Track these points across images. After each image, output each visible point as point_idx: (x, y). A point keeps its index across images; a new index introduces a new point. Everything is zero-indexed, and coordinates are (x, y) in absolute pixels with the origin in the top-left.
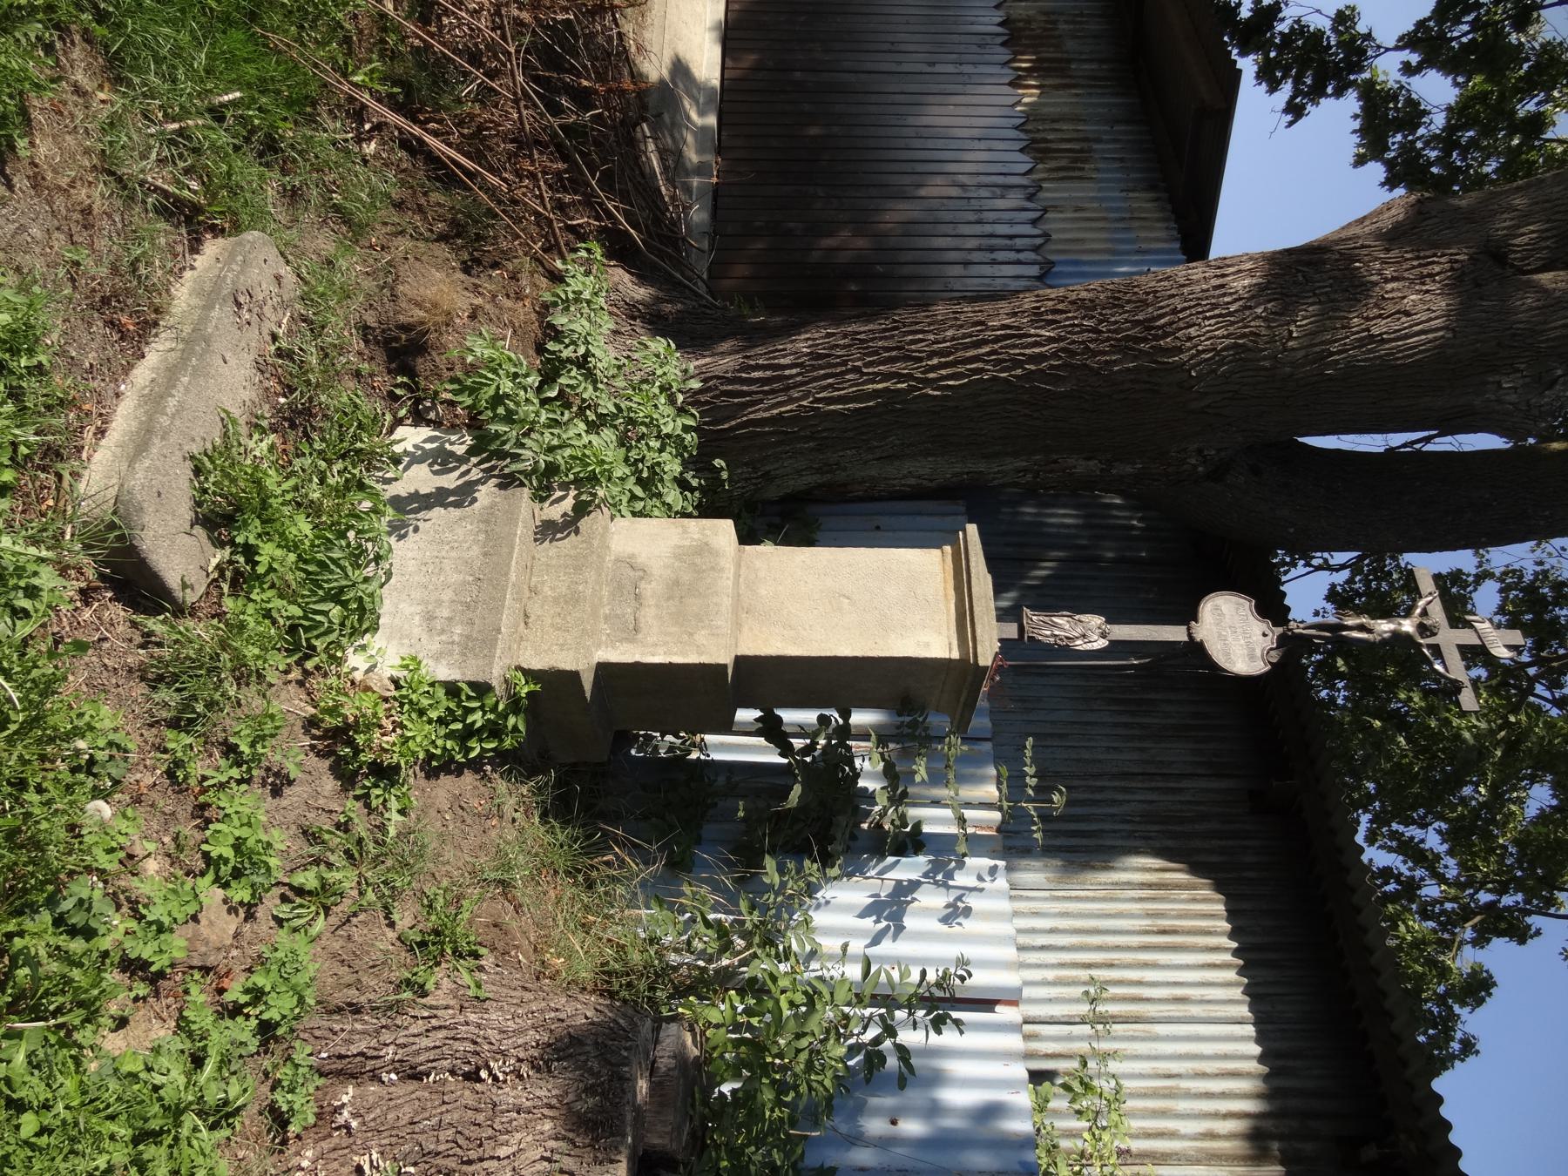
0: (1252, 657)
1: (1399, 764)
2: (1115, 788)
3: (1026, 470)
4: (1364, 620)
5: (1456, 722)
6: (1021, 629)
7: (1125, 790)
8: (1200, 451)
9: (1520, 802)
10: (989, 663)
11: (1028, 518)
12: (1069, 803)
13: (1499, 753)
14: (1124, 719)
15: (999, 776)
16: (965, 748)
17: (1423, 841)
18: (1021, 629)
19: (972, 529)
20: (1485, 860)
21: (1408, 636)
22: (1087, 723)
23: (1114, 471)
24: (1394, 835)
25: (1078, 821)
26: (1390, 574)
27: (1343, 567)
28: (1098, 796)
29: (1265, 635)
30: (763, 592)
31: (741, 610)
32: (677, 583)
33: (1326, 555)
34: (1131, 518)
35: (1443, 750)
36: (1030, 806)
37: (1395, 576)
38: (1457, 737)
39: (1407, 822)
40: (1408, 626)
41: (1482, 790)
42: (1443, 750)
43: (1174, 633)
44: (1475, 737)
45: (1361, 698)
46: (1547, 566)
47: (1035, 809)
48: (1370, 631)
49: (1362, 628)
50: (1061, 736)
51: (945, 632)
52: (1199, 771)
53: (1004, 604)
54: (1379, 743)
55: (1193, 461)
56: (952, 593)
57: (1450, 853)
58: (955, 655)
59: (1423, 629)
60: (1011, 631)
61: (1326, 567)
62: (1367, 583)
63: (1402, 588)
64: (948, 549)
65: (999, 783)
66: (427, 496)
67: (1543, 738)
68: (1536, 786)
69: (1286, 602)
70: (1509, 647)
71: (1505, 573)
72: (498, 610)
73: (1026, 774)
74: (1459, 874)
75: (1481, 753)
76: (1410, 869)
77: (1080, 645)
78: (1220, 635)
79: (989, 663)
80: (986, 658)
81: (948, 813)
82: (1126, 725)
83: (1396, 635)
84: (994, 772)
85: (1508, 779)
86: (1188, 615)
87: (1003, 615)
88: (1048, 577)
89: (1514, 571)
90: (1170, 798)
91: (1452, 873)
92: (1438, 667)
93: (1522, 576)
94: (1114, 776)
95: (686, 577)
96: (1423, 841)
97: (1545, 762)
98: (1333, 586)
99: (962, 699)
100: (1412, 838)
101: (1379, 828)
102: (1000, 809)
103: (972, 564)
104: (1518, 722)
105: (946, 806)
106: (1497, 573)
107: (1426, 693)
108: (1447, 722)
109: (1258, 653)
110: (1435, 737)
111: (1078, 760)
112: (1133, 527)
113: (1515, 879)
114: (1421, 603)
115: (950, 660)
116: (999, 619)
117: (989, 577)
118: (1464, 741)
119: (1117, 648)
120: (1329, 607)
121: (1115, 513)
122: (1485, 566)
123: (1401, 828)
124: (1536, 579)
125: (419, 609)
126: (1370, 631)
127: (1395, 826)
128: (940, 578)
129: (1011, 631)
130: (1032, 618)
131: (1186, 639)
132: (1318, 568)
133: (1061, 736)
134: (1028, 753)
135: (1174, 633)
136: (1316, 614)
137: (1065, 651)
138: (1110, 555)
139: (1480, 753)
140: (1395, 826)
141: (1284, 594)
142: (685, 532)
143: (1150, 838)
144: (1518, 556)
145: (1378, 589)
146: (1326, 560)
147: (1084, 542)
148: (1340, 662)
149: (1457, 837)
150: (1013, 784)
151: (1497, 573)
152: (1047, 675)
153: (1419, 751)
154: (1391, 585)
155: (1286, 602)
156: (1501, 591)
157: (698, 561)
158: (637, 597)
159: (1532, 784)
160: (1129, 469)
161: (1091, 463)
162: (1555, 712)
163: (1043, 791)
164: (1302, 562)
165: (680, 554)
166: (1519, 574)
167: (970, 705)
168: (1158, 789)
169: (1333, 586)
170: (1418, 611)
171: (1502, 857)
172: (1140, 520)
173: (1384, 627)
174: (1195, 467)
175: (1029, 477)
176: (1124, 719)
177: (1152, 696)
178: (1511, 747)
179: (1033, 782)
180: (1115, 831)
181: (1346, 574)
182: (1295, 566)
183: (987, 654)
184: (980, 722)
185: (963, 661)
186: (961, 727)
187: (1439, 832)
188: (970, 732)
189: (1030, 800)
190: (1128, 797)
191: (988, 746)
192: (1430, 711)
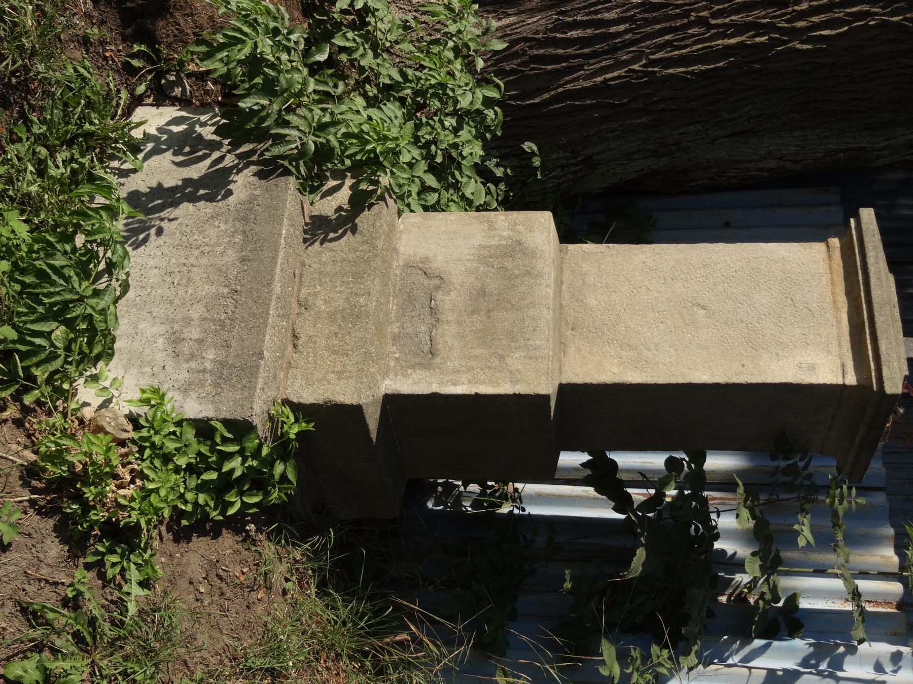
16: (861, 501)
30: (592, 301)
31: (565, 325)
32: (482, 292)
51: (834, 347)
56: (842, 300)
58: (851, 379)
66: (173, 190)
72: (260, 330)
80: (894, 385)
81: (838, 584)
95: (494, 286)
99: (858, 439)
103: (871, 260)
105: (836, 576)
115: (844, 387)
117: (892, 278)
125: (163, 329)
128: (826, 279)
142: (491, 227)
157: (509, 264)
158: (433, 311)
165: (486, 256)
185: (862, 388)
188: (866, 482)
191: (880, 499)
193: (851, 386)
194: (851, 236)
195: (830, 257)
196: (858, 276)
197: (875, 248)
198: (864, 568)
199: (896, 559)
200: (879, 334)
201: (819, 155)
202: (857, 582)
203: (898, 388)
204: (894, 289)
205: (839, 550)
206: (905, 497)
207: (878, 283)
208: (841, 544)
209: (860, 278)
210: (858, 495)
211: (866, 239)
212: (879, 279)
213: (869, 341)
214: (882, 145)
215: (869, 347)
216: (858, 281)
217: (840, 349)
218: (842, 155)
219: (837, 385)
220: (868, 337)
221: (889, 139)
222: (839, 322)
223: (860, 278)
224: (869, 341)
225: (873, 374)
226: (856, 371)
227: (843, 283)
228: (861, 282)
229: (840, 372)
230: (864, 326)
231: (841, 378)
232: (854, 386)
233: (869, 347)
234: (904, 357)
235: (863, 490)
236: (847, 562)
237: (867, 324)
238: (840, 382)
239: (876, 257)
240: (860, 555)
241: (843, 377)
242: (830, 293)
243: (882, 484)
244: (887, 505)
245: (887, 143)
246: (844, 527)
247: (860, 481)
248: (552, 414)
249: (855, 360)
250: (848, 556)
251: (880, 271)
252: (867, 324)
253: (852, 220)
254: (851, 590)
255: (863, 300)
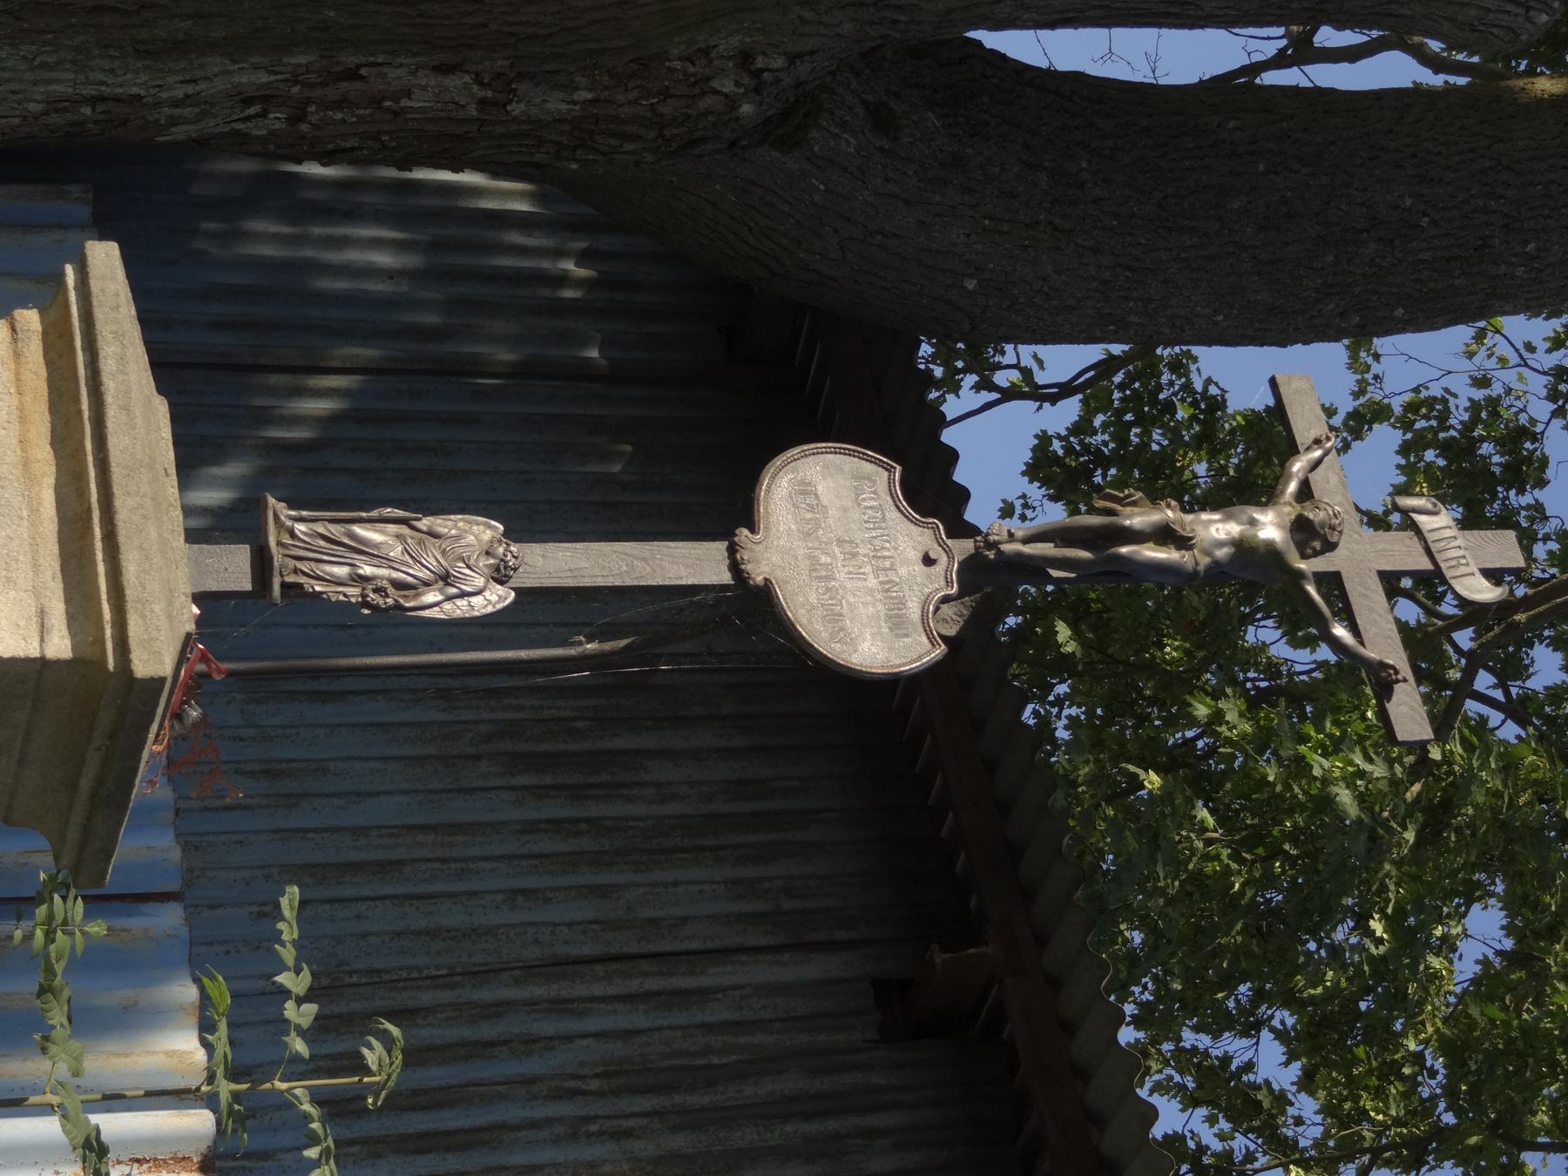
0: (897, 622)
1: (1198, 877)
2: (532, 1004)
3: (266, 99)
4: (1169, 514)
5: (1319, 765)
6: (262, 563)
7: (559, 1006)
8: (745, 58)
9: (1447, 946)
10: (165, 667)
11: (269, 251)
12: (415, 1056)
13: (1410, 836)
14: (555, 809)
15: (205, 1000)
16: (97, 928)
17: (1249, 1066)
18: (262, 563)
19: (105, 256)
20: (1379, 1093)
21: (1271, 553)
22: (456, 828)
23: (516, 109)
24: (1185, 1058)
25: (437, 1105)
26: (1169, 408)
27: (1065, 390)
28: (487, 1031)
29: (928, 561)
33: (1026, 352)
34: (559, 254)
35: (1292, 837)
36: (299, 1090)
37: (1182, 413)
38: (1325, 803)
39: (1218, 1024)
40: (1270, 527)
41: (1377, 926)
42: (1292, 837)
43: (693, 564)
44: (1361, 799)
45: (1108, 720)
46: (1497, 389)
47: (318, 1098)
48: (1183, 543)
49: (1165, 535)
50: (383, 868)
52: (756, 939)
53: (211, 497)
54: (1153, 830)
55: (727, 86)
57: (1307, 1083)
58: (60, 646)
59: (1306, 533)
60: (231, 568)
61: (1033, 391)
62: (1120, 431)
63: (1199, 442)
64: (30, 318)
65: (206, 1027)
67: (1497, 794)
68: (1476, 907)
69: (960, 476)
70: (1494, 576)
71: (1412, 407)
73: (284, 993)
74: (1327, 1135)
75: (1374, 837)
76: (1222, 1137)
77: (434, 603)
78: (814, 564)
79: (165, 667)
80: (155, 651)
81: (48, 1127)
82: (556, 826)
83: (1244, 549)
84: (190, 993)
85: (1436, 895)
86: (729, 511)
87: (206, 529)
88: (333, 419)
89: (1431, 402)
90: (678, 1018)
91: (1308, 1136)
92: (1340, 631)
93: (1444, 416)
94: (527, 971)
96: (1249, 1066)
97: (1508, 851)
98: (1044, 439)
99: (85, 784)
100: (1226, 1059)
101: (1154, 1042)
102: (211, 1102)
103: (108, 365)
104: (1448, 759)
105: (46, 1109)
106: (1397, 405)
107: (1254, 703)
108: (1299, 767)
109: (913, 610)
110: (1277, 806)
111: (432, 934)
112: (563, 280)
113: (1439, 1132)
114: (1298, 466)
115: (42, 663)
116: (192, 536)
117: (161, 407)
118: (1340, 816)
119: (540, 608)
120: (1035, 492)
121: (515, 237)
122: (1374, 394)
123: (1204, 1041)
124: (1475, 419)
126: (1183, 543)
127: (1189, 1038)
129: (231, 568)
130: (293, 528)
131: (726, 578)
132: (1009, 394)
133: (383, 868)
134: (288, 931)
135: (693, 564)
136: (1007, 511)
137: (390, 621)
138: (506, 356)
139: (1373, 838)
140: (1189, 1038)
141: (952, 456)
143: (627, 1134)
144: (1426, 360)
145: (1144, 446)
146: (1027, 373)
147: (431, 319)
148: (1063, 632)
149: (1316, 1044)
150: (246, 1029)
151: (1397, 405)
152: (341, 696)
153: (1247, 841)
154: (1174, 433)
155: (960, 476)
156: (1404, 449)
159: (1468, 905)
160: (556, 104)
161: (454, 82)
162: (1510, 731)
163: (339, 1027)
164: (970, 379)
166: (1438, 407)
167: (112, 798)
168: (648, 996)
169: (1044, 439)
170: (1293, 487)
171: (1412, 1083)
172: (583, 258)
173: (1217, 530)
174: (732, 102)
175: (277, 119)
176: (555, 809)
177: (625, 741)
178: (1436, 816)
179: (300, 1014)
180: (534, 1125)
181: (1070, 410)
182: (956, 389)
183: (157, 642)
184: (145, 848)
185: (83, 665)
186: (85, 870)
187: (1281, 1035)
188: (112, 881)
189: (298, 1069)
190: (569, 1025)
191: (169, 918)
192: (1263, 741)
193: (58, 662)
194: (67, 306)
195: (17, 355)
196: (78, 401)
197: (118, 336)
198: (112, 1087)
199: (201, 1055)
200: (122, 539)
201: (34, 107)
202: (95, 1119)
203: (161, 663)
204: (166, 433)
205: (53, 1049)
206: (255, 909)
207: (124, 418)
208: (58, 1033)
209: (85, 406)
210: (88, 915)
211: (99, 315)
212: (126, 409)
213: (99, 556)
214: (179, 93)
215: (101, 568)
216: (80, 412)
217: (36, 573)
218: (87, 111)
219: (27, 661)
220: (98, 545)
221: (194, 81)
222: (34, 510)
223: (85, 406)
224: (99, 556)
225: (108, 632)
226: (70, 626)
227: (47, 418)
228: (86, 414)
229: (35, 627)
230: (90, 518)
231: (36, 644)
232: (66, 663)
233: (101, 568)
234: (185, 588)
235: (98, 902)
236: (76, 1074)
237: (96, 515)
238: (33, 651)
239: (121, 359)
240: (119, 1055)
241: (42, 640)
242: (15, 441)
243: (173, 886)
244: (184, 932)
245: (190, 89)
246: (66, 993)
247: (100, 881)
248: (623, 643)
249: (68, 600)
250: (78, 1059)
251: (128, 392)
252: (96, 515)
253: (70, 271)
254: (80, 1140)
255: (90, 458)
